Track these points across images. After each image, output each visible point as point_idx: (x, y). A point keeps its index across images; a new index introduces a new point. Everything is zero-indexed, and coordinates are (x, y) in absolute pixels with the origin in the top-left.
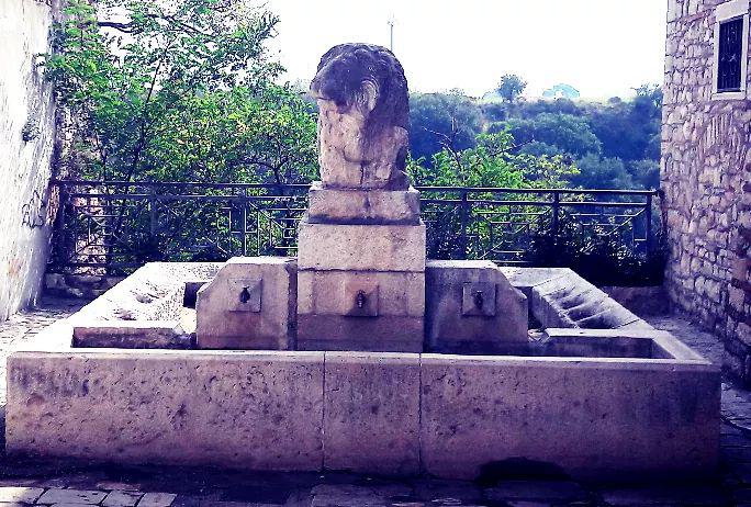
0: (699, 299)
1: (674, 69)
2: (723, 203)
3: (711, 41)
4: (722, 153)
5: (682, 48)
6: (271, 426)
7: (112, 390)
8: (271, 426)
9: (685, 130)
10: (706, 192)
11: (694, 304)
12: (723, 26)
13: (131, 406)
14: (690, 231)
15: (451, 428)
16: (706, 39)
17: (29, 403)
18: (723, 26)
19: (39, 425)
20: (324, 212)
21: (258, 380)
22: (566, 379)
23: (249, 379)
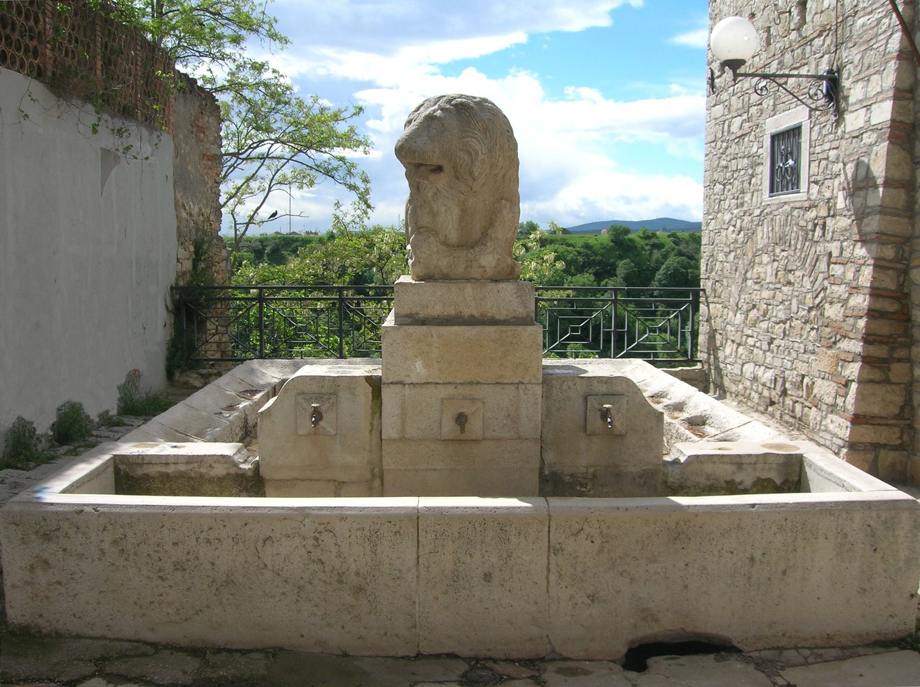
0: (748, 383)
1: (715, 182)
2: (779, 297)
3: (760, 151)
4: (778, 251)
5: (724, 163)
6: (350, 599)
7: (136, 554)
8: (350, 599)
9: (731, 234)
10: (757, 287)
11: (741, 387)
12: (774, 137)
13: (161, 574)
14: (736, 322)
15: (588, 596)
16: (755, 149)
17: (32, 568)
18: (774, 137)
19: (47, 597)
20: (414, 311)
21: (326, 538)
22: (739, 527)
23: (316, 539)
